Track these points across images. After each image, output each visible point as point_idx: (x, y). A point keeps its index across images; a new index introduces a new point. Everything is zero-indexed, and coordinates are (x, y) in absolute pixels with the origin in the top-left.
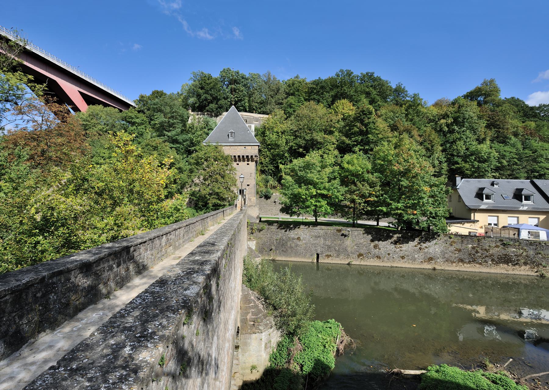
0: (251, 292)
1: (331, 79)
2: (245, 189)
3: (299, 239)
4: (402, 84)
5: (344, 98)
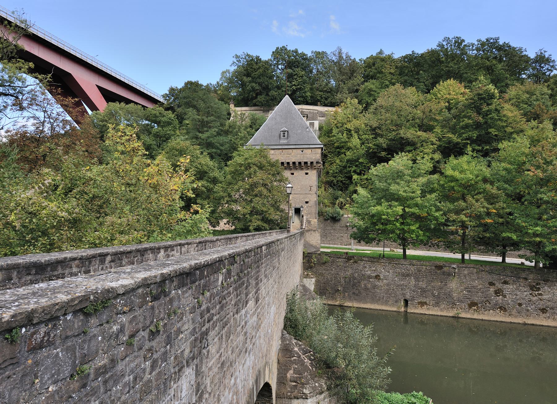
0: (294, 341)
1: (432, 53)
2: (302, 207)
3: (377, 277)
4: (545, 52)
5: (449, 77)
